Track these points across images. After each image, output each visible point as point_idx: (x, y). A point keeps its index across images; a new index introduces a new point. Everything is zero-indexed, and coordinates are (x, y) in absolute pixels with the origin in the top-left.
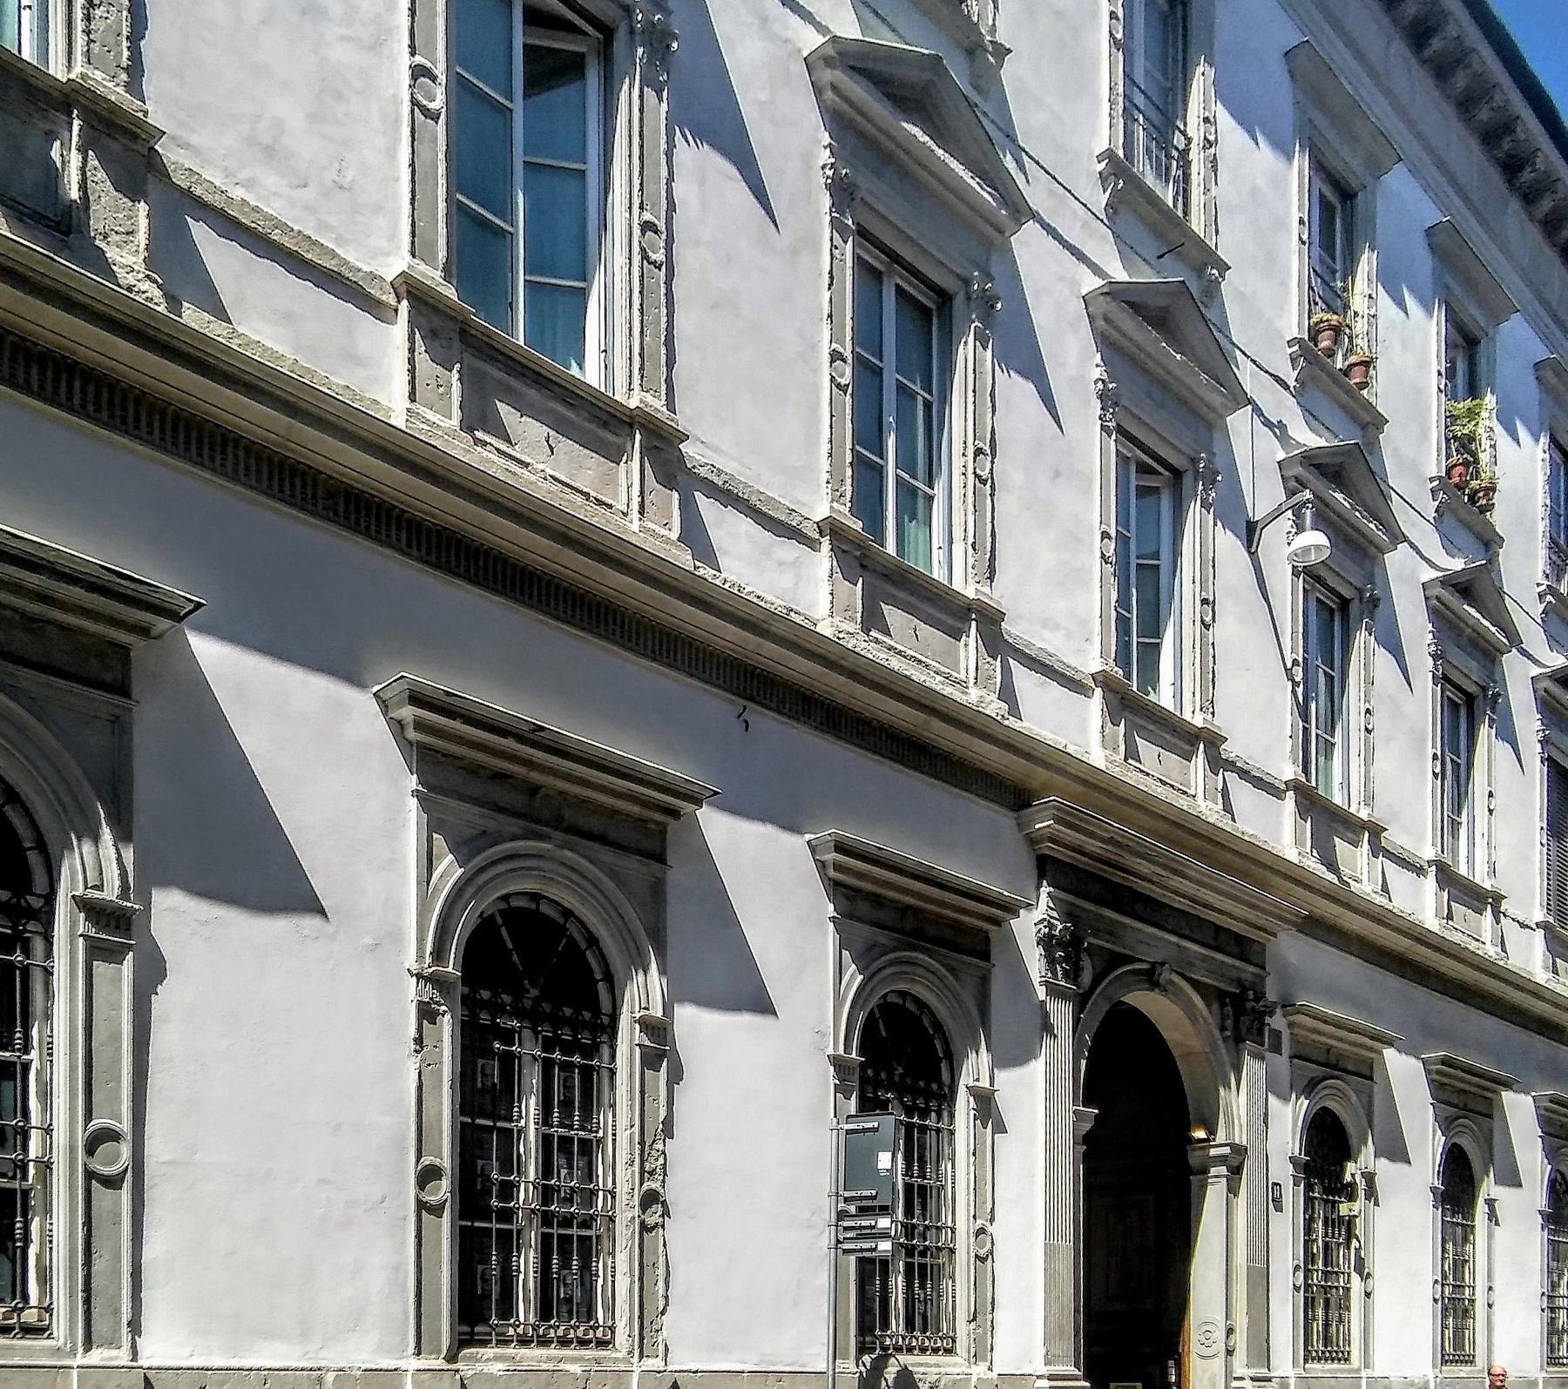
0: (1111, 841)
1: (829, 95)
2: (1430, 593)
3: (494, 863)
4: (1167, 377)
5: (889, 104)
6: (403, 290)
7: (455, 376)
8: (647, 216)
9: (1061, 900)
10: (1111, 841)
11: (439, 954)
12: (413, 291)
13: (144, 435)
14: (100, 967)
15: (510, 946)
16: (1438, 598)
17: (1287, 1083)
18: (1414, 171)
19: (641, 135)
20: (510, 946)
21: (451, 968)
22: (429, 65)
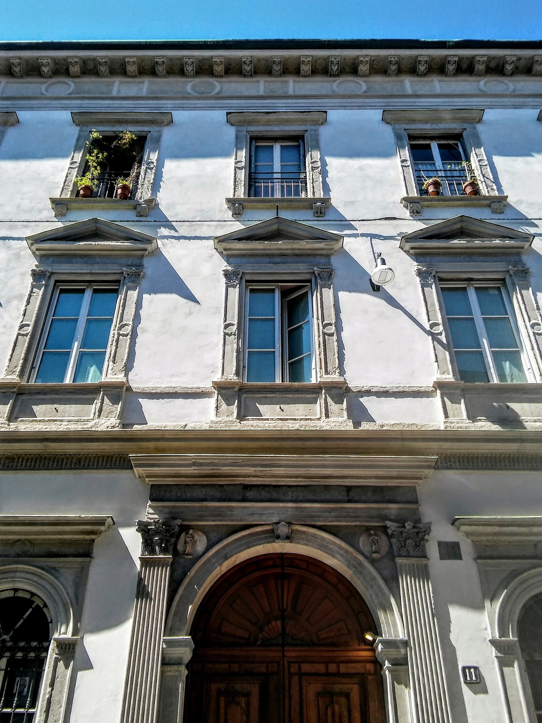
0: (194, 464)
1: (411, 251)
2: (221, 249)
3: (27, 573)
4: (281, 251)
5: (63, 242)
6: (436, 386)
7: (463, 405)
8: (533, 321)
9: (157, 507)
10: (194, 464)
11: (503, 632)
12: (440, 385)
13: (454, 467)
14: (505, 669)
15: (30, 610)
16: (412, 248)
17: (479, 595)
18: (334, 108)
19: (524, 303)
20: (30, 610)
21: (512, 637)
22: (436, 322)
